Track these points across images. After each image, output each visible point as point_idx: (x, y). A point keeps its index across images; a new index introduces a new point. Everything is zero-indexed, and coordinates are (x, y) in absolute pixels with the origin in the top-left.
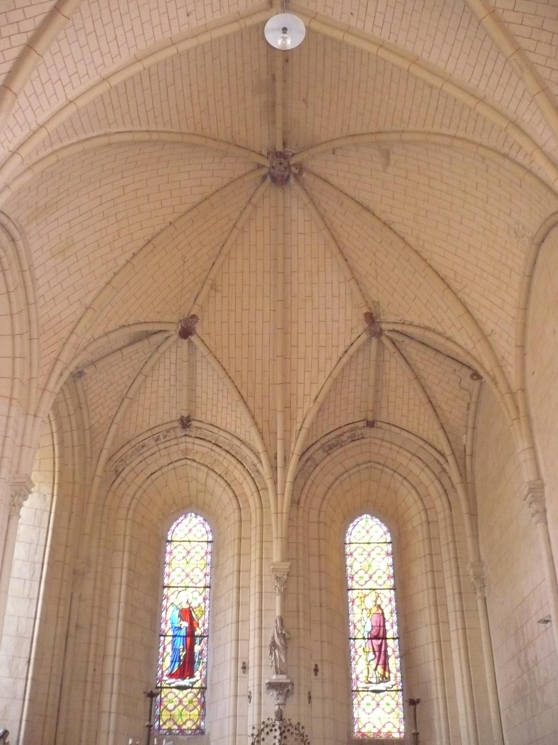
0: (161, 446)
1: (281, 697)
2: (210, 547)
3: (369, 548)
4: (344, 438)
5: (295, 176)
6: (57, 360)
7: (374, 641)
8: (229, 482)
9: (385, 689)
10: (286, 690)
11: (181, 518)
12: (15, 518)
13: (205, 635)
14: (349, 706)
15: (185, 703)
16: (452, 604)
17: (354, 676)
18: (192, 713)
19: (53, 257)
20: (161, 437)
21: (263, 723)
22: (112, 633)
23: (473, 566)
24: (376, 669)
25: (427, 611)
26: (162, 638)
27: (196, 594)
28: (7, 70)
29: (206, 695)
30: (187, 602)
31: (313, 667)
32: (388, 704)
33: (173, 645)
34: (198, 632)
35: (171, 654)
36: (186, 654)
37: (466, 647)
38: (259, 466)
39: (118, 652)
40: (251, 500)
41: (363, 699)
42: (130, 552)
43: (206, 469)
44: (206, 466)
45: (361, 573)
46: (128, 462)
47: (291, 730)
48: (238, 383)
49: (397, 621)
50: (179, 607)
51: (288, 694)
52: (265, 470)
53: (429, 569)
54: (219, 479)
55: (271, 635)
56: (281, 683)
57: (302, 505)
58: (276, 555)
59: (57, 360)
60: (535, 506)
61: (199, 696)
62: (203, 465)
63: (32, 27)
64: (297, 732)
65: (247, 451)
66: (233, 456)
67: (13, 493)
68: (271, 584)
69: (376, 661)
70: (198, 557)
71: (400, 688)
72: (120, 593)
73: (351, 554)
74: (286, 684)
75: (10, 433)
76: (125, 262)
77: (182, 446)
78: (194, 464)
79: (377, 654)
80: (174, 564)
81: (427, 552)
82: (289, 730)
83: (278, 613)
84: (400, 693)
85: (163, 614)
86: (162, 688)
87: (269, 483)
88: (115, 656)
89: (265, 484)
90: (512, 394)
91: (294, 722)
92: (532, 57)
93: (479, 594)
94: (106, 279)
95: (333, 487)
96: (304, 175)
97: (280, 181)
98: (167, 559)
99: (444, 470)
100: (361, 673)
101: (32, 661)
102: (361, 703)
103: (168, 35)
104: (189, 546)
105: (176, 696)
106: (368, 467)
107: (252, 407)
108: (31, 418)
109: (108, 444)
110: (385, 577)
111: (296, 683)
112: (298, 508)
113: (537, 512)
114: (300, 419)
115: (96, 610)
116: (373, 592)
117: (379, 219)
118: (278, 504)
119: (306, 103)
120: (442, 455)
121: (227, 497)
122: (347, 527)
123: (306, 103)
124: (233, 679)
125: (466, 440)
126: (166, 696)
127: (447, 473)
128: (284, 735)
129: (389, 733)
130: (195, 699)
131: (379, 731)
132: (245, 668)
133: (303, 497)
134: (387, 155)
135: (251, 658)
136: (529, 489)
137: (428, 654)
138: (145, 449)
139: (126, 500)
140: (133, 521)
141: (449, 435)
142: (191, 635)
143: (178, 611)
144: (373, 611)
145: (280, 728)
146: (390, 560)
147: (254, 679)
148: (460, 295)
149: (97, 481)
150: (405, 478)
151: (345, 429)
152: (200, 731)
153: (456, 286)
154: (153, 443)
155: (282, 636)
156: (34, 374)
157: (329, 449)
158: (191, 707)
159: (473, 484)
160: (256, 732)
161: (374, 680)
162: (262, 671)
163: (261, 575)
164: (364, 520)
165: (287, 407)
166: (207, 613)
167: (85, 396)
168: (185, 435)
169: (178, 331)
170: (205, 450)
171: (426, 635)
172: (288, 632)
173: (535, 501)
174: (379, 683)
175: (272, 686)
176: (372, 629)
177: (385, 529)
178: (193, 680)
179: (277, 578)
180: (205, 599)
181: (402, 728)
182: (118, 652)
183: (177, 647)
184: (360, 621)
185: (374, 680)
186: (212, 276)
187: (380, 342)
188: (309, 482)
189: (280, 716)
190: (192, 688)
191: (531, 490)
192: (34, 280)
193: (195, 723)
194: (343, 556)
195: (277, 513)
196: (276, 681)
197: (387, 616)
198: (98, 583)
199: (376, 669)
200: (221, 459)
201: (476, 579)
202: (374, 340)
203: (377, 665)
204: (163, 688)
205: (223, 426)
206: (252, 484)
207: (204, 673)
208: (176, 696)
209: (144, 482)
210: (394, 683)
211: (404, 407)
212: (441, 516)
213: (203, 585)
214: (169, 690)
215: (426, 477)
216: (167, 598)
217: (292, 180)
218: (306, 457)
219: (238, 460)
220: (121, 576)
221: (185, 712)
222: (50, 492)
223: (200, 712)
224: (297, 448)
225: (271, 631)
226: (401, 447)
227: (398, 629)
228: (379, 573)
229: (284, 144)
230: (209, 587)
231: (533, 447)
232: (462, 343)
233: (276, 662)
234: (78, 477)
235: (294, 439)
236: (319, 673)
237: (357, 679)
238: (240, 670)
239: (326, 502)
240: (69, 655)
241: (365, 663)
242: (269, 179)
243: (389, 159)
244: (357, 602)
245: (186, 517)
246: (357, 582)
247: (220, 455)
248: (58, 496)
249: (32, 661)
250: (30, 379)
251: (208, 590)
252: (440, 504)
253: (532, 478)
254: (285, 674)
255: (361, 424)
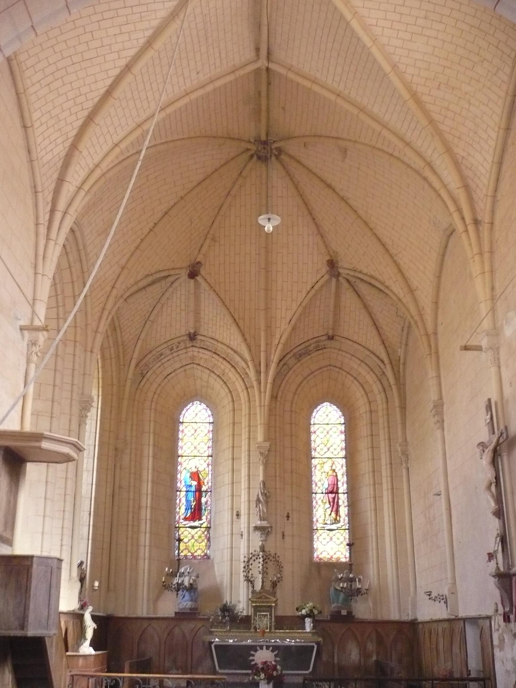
0: (175, 354)
1: (263, 536)
2: (211, 426)
3: (328, 428)
4: (311, 348)
5: (275, 155)
6: (104, 309)
7: (330, 495)
8: (225, 381)
9: (336, 528)
10: (266, 532)
11: (189, 406)
12: (83, 425)
13: (209, 490)
14: (311, 540)
15: (196, 538)
16: (385, 472)
17: (315, 520)
18: (201, 544)
19: (99, 236)
20: (174, 347)
21: (252, 553)
22: (144, 491)
23: (400, 445)
24: (330, 515)
25: (367, 476)
26: (178, 493)
27: (202, 462)
28: (75, 134)
29: (210, 532)
30: (196, 467)
31: (286, 515)
32: (338, 539)
33: (186, 498)
34: (204, 488)
35: (185, 504)
36: (195, 504)
37: (393, 502)
38: (247, 370)
39: (149, 505)
40: (241, 395)
41: (321, 535)
42: (154, 433)
43: (208, 372)
44: (208, 369)
45: (322, 446)
46: (151, 366)
47: (271, 558)
48: (232, 310)
49: (347, 481)
50: (190, 470)
51: (268, 534)
52: (252, 373)
53: (370, 445)
54: (218, 379)
55: (257, 494)
56: (264, 527)
57: (279, 399)
58: (260, 438)
59: (104, 309)
60: (437, 418)
61: (206, 533)
62: (206, 368)
63: (92, 105)
64: (274, 559)
65: (238, 359)
66: (229, 362)
67: (81, 408)
68: (256, 457)
69: (331, 509)
70: (203, 434)
71: (347, 527)
72: (148, 463)
73: (315, 432)
74: (267, 527)
75: (77, 367)
76: (149, 230)
77: (190, 354)
78: (199, 367)
79: (332, 504)
80: (186, 439)
81: (369, 433)
82: (269, 558)
83: (261, 478)
84: (347, 531)
85: (179, 476)
86: (179, 528)
87: (255, 384)
88: (147, 507)
89: (252, 383)
90: (427, 335)
91: (273, 553)
92: (441, 127)
93: (404, 465)
94: (136, 245)
95: (302, 385)
96: (283, 157)
97: (263, 159)
98: (180, 436)
99: (384, 373)
100: (320, 517)
101: (92, 513)
102: (319, 538)
103: (183, 88)
104: (196, 425)
105: (190, 533)
106: (328, 370)
107: (242, 327)
108: (89, 354)
109: (136, 355)
110: (339, 449)
111: (274, 527)
112: (276, 402)
113: (438, 421)
114: (278, 336)
115: (132, 476)
116: (330, 460)
117: (338, 194)
118: (261, 399)
119: (284, 110)
120: (383, 362)
121: (223, 392)
122: (312, 412)
123: (284, 110)
124: (230, 523)
125: (400, 352)
126: (182, 533)
127: (386, 375)
128: (265, 561)
129: (338, 559)
130: (203, 535)
131: (332, 557)
132: (238, 515)
133: (280, 394)
134: (344, 152)
135: (242, 509)
136: (434, 406)
137: (367, 505)
138: (163, 357)
139: (150, 394)
140: (155, 410)
141: (388, 349)
142: (199, 490)
143: (189, 474)
144: (329, 474)
145: (263, 557)
146: (343, 437)
147: (244, 523)
148: (396, 258)
149: (129, 383)
150: (355, 378)
151: (311, 342)
152: (207, 557)
153: (393, 251)
154: (168, 352)
155: (264, 494)
156: (89, 322)
157: (299, 357)
158: (200, 540)
159: (404, 385)
160: (246, 560)
161: (329, 522)
162: (249, 518)
163: (249, 451)
164: (325, 407)
165: (268, 327)
166: (210, 475)
167: (119, 322)
168: (193, 346)
169: (187, 274)
170: (206, 357)
171: (366, 492)
172: (269, 492)
173: (437, 414)
174: (332, 524)
175: (256, 528)
176: (329, 486)
177: (340, 413)
178: (201, 522)
179: (261, 453)
180: (208, 465)
181: (348, 555)
182: (149, 505)
183: (189, 499)
184: (320, 481)
185: (329, 522)
186: (212, 232)
187: (338, 280)
188: (284, 382)
189: (263, 549)
190: (200, 527)
191: (435, 406)
192: (86, 255)
193: (203, 552)
194: (309, 433)
195: (260, 406)
196: (260, 525)
197: (340, 477)
198: (133, 456)
199: (330, 515)
200: (219, 364)
201: (402, 454)
202: (334, 280)
203: (332, 511)
204: (181, 527)
205: (220, 340)
206: (243, 384)
207: (209, 517)
208: (190, 533)
209: (163, 381)
210: (343, 524)
211: (355, 325)
212: (380, 407)
213: (207, 455)
214: (185, 529)
215: (370, 378)
216: (181, 464)
217: (273, 158)
218: (282, 363)
219: (232, 365)
220: (149, 451)
221: (196, 544)
222: (97, 394)
223: (206, 544)
224: (275, 358)
225: (257, 491)
226: (353, 355)
227: (347, 486)
228: (335, 446)
229: (267, 135)
230: (212, 456)
231: (439, 377)
232: (396, 292)
233: (260, 512)
234: (115, 381)
235: (273, 352)
236: (290, 519)
237: (317, 521)
238: (235, 516)
239: (296, 396)
240: (116, 508)
241: (323, 510)
242: (255, 158)
243: (346, 154)
244: (318, 467)
245: (193, 404)
246: (319, 453)
247: (218, 361)
248: (102, 396)
249: (92, 513)
250: (86, 325)
251: (210, 458)
252: (380, 398)
253: (436, 398)
254: (266, 520)
255: (324, 338)
